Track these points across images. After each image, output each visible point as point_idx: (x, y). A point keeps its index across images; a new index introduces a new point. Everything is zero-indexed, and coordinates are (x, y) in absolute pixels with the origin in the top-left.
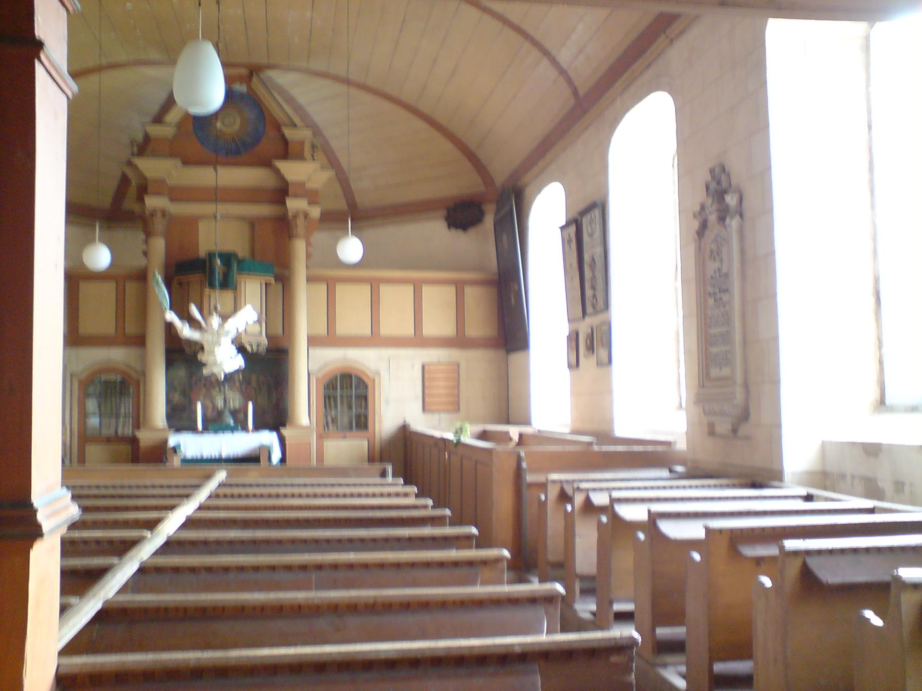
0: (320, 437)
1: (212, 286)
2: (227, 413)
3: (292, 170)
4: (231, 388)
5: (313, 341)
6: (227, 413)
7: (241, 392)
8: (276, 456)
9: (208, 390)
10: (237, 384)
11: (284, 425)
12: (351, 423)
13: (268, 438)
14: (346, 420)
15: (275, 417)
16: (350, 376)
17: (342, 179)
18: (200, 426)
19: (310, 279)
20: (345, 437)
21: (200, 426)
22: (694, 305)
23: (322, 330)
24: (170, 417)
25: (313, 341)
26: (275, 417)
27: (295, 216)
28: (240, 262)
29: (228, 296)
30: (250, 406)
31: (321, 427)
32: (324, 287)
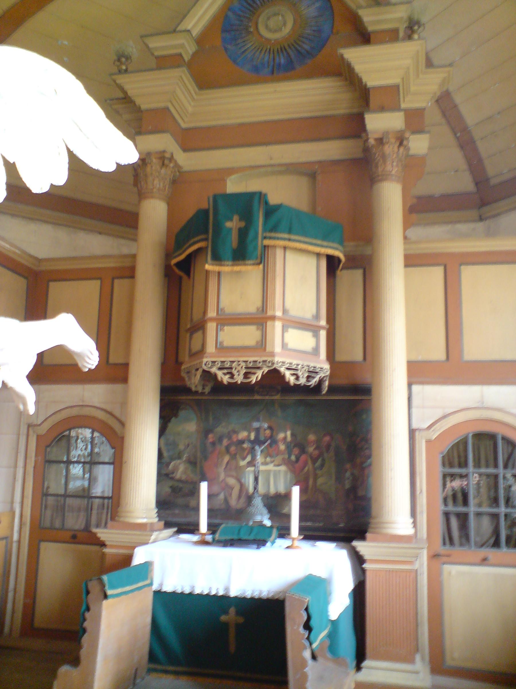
0: (434, 556)
1: (217, 258)
2: (258, 502)
3: (372, 64)
4: (267, 454)
5: (419, 372)
6: (258, 502)
7: (287, 462)
8: (339, 604)
9: (234, 457)
10: (282, 447)
11: (361, 535)
12: (496, 532)
13: (330, 562)
14: (486, 524)
15: (344, 515)
16: (492, 437)
17: (466, 142)
18: (203, 527)
19: (411, 261)
20: (484, 561)
21: (203, 527)
22: (374, 511)
23: (438, 353)
24: (163, 504)
25: (419, 372)
26: (344, 515)
27: (380, 141)
28: (271, 211)
29: (251, 273)
30: (296, 491)
31: (439, 540)
32: (438, 272)
